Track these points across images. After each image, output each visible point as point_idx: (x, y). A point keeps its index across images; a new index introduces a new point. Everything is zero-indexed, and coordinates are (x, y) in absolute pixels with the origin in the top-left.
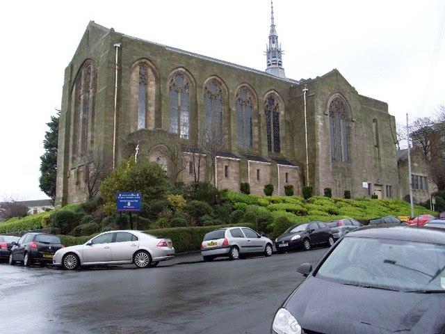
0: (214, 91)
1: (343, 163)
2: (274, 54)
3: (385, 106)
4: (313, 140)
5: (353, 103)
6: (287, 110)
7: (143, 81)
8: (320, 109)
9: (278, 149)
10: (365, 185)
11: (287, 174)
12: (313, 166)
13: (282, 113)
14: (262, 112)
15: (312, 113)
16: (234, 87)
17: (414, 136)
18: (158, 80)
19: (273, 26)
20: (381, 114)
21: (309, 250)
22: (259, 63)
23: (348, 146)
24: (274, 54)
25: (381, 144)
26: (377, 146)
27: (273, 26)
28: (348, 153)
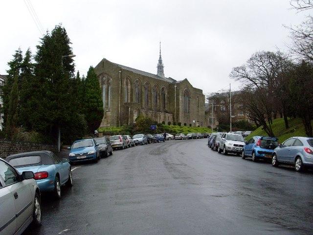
0: (146, 86)
1: (187, 112)
2: (160, 67)
3: (202, 91)
4: (178, 105)
5: (192, 91)
6: (168, 93)
7: (127, 84)
8: (181, 94)
9: (164, 107)
10: (194, 121)
11: (169, 117)
12: (178, 114)
13: (166, 94)
14: (161, 94)
15: (178, 95)
16: (153, 85)
17: (210, 99)
18: (131, 84)
19: (160, 56)
20: (200, 95)
21: (273, 166)
22: (154, 71)
23: (189, 107)
24: (160, 67)
25: (200, 106)
26: (198, 107)
27: (160, 56)
28: (189, 110)
